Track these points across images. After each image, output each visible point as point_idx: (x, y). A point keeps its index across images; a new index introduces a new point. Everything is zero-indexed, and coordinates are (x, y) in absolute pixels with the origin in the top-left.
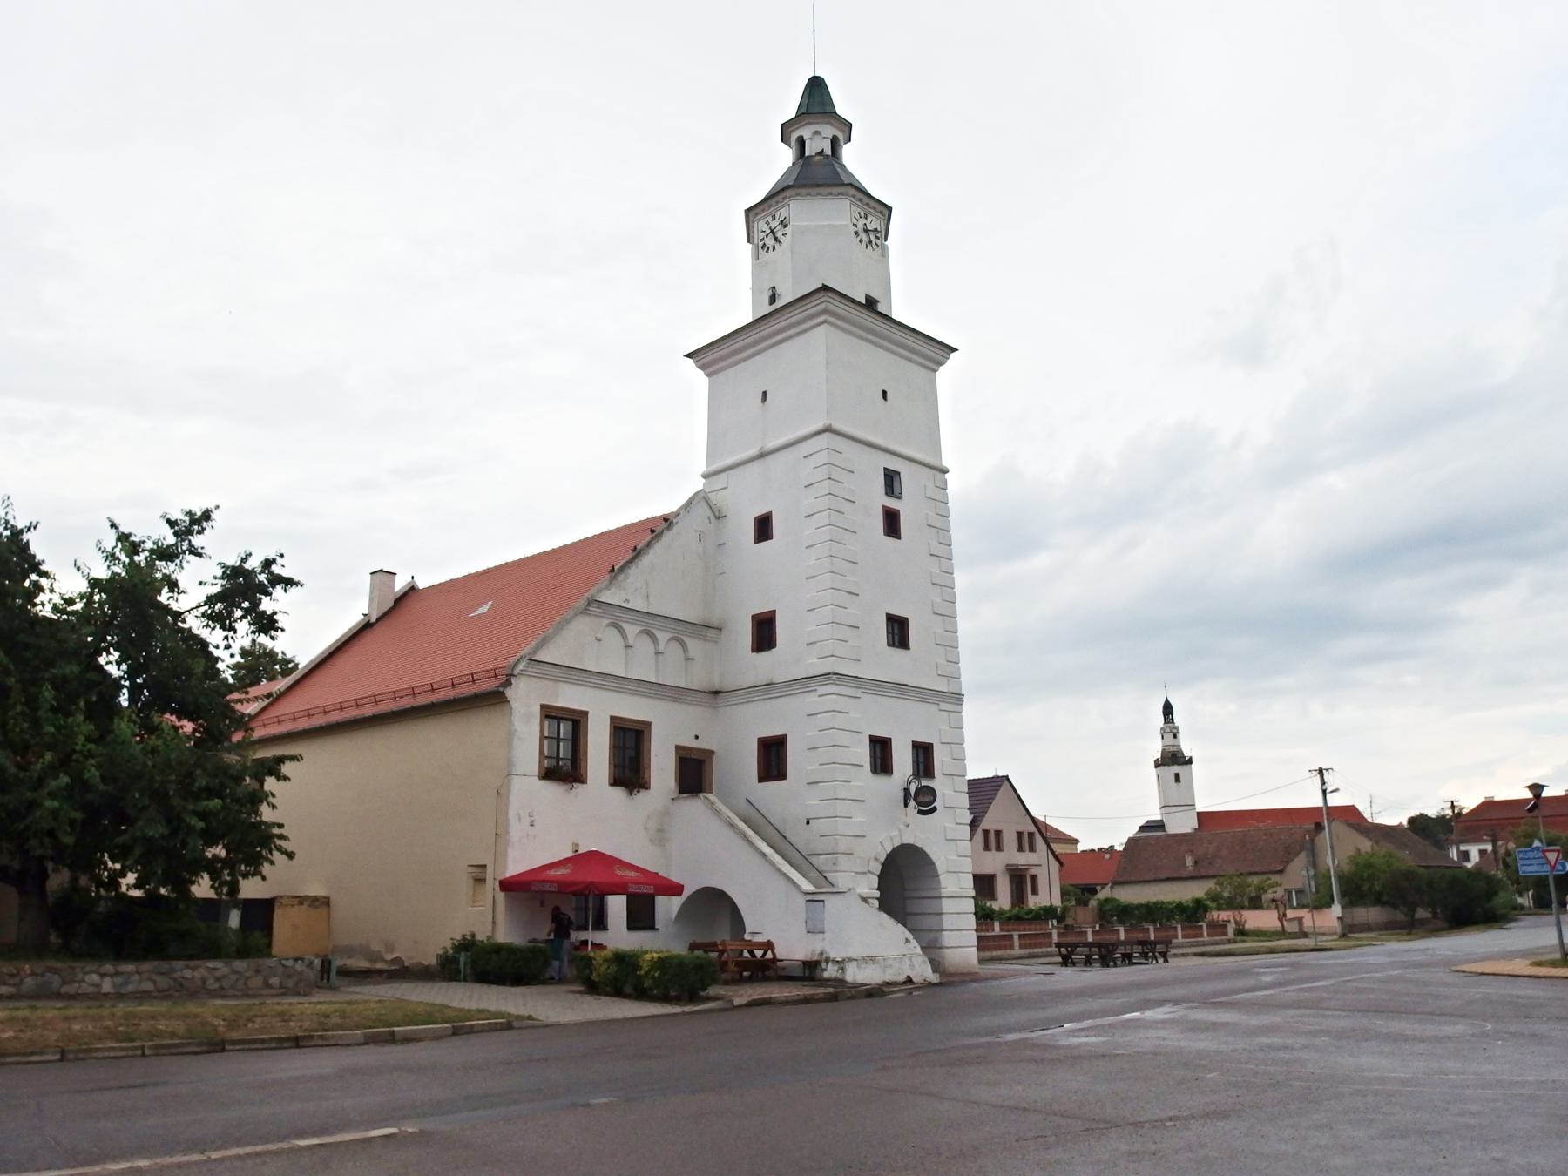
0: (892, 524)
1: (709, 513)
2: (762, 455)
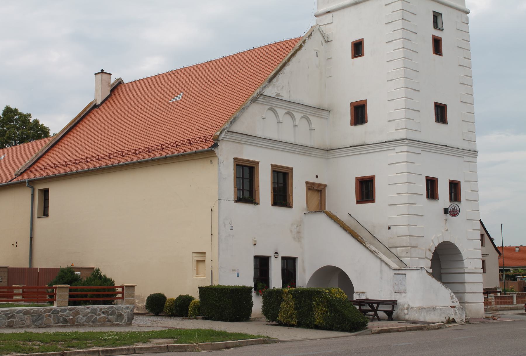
0: (437, 46)
1: (322, 39)
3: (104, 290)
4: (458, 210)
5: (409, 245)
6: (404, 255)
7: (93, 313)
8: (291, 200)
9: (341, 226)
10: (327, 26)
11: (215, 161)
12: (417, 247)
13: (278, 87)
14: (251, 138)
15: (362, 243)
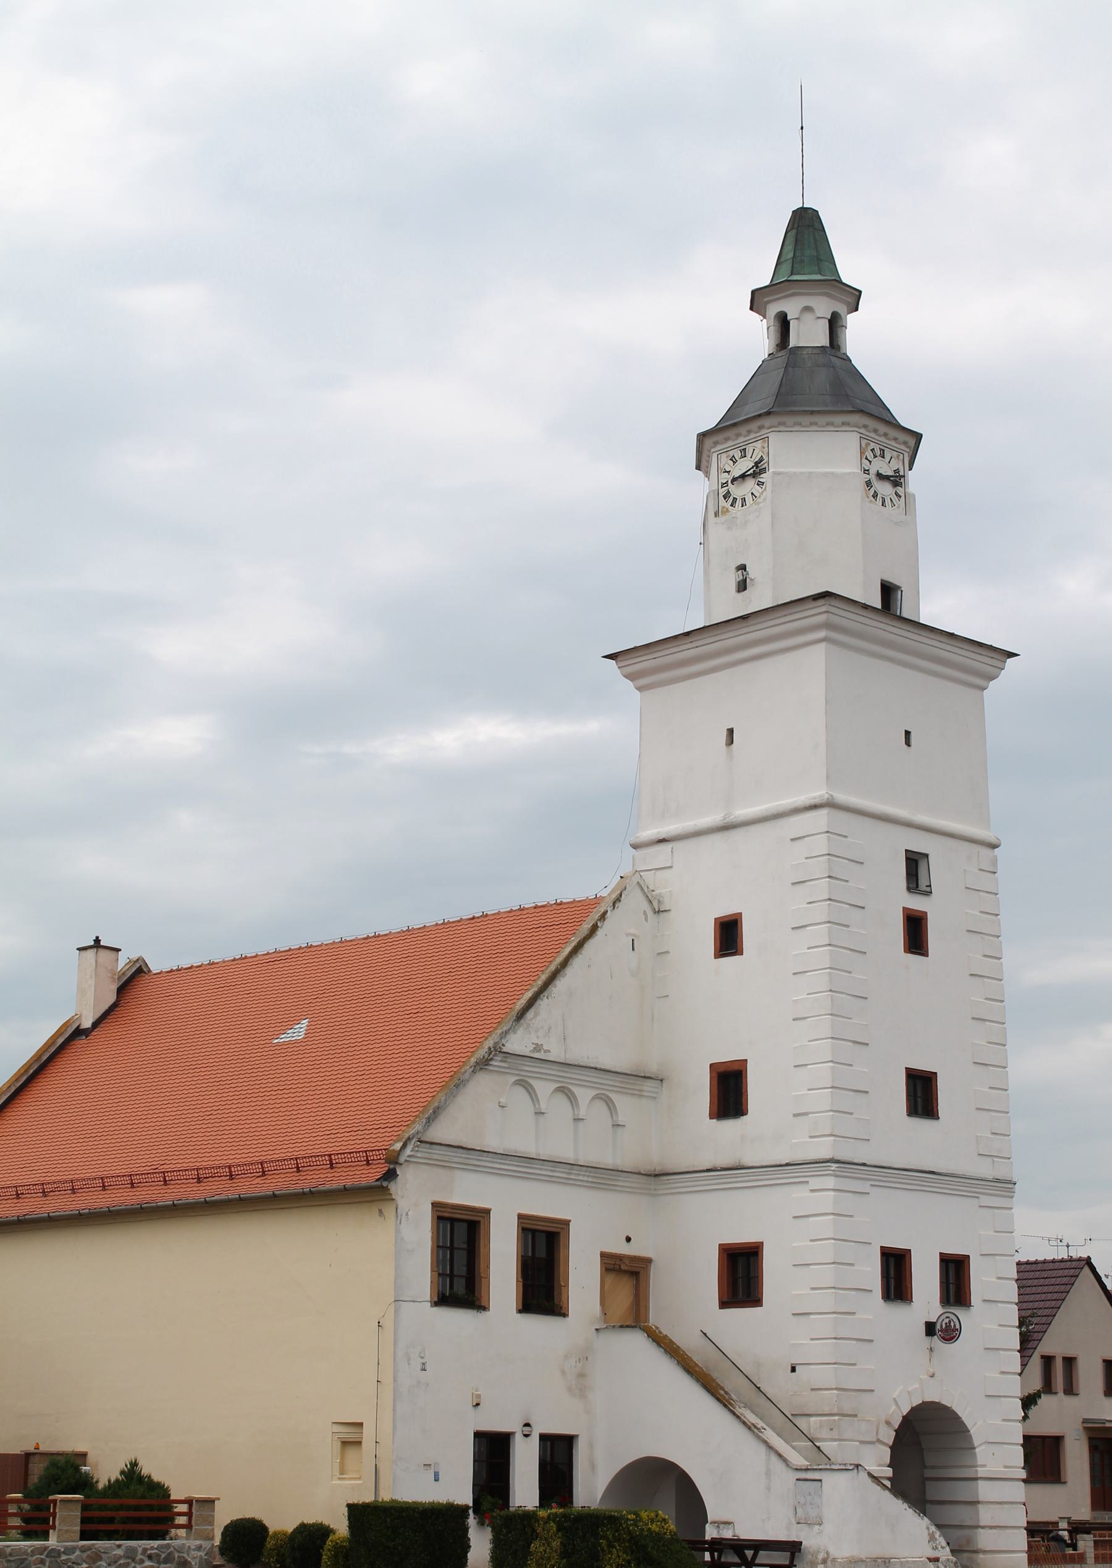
1: (645, 905)
2: (726, 827)
3: (151, 1508)
4: (958, 1327)
5: (835, 1411)
6: (824, 1434)
7: (128, 1557)
8: (564, 1299)
9: (679, 1363)
10: (658, 872)
11: (389, 1210)
12: (856, 1416)
13: (537, 1031)
14: (473, 1155)
15: (725, 1406)
